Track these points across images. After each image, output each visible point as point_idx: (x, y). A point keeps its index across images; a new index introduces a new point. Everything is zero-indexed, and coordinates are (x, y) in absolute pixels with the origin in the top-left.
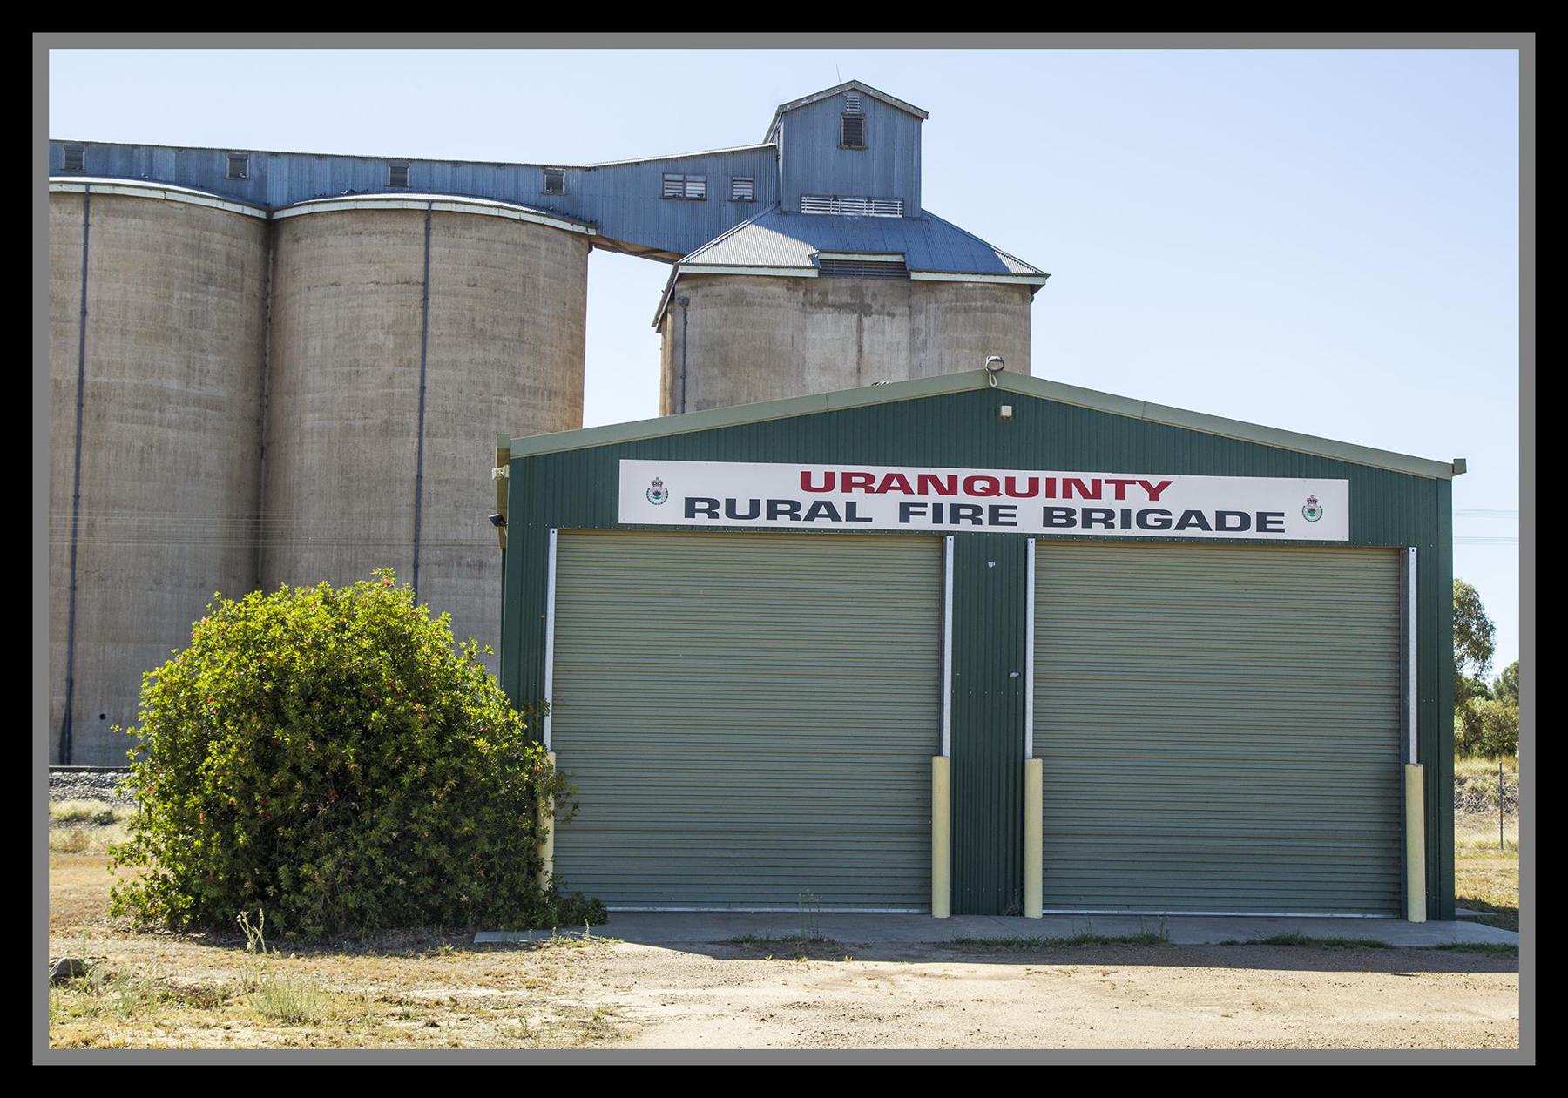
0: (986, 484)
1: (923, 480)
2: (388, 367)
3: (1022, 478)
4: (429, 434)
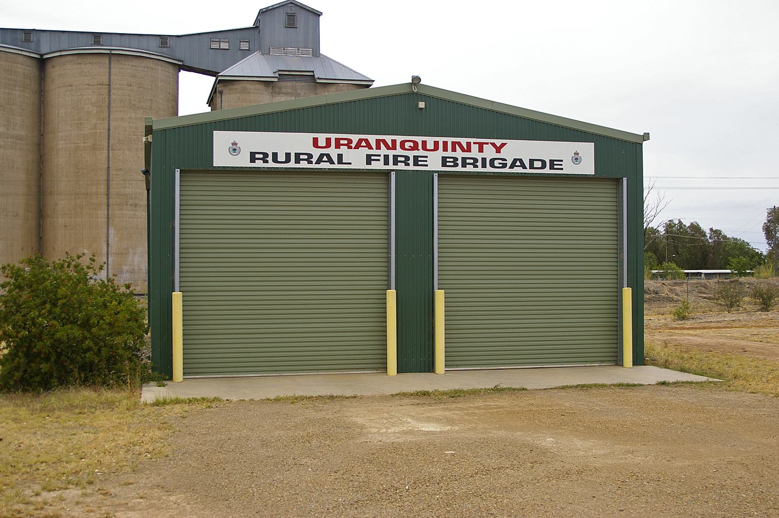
0: (412, 144)
1: (378, 142)
2: (94, 121)
3: (430, 141)
4: (112, 149)
